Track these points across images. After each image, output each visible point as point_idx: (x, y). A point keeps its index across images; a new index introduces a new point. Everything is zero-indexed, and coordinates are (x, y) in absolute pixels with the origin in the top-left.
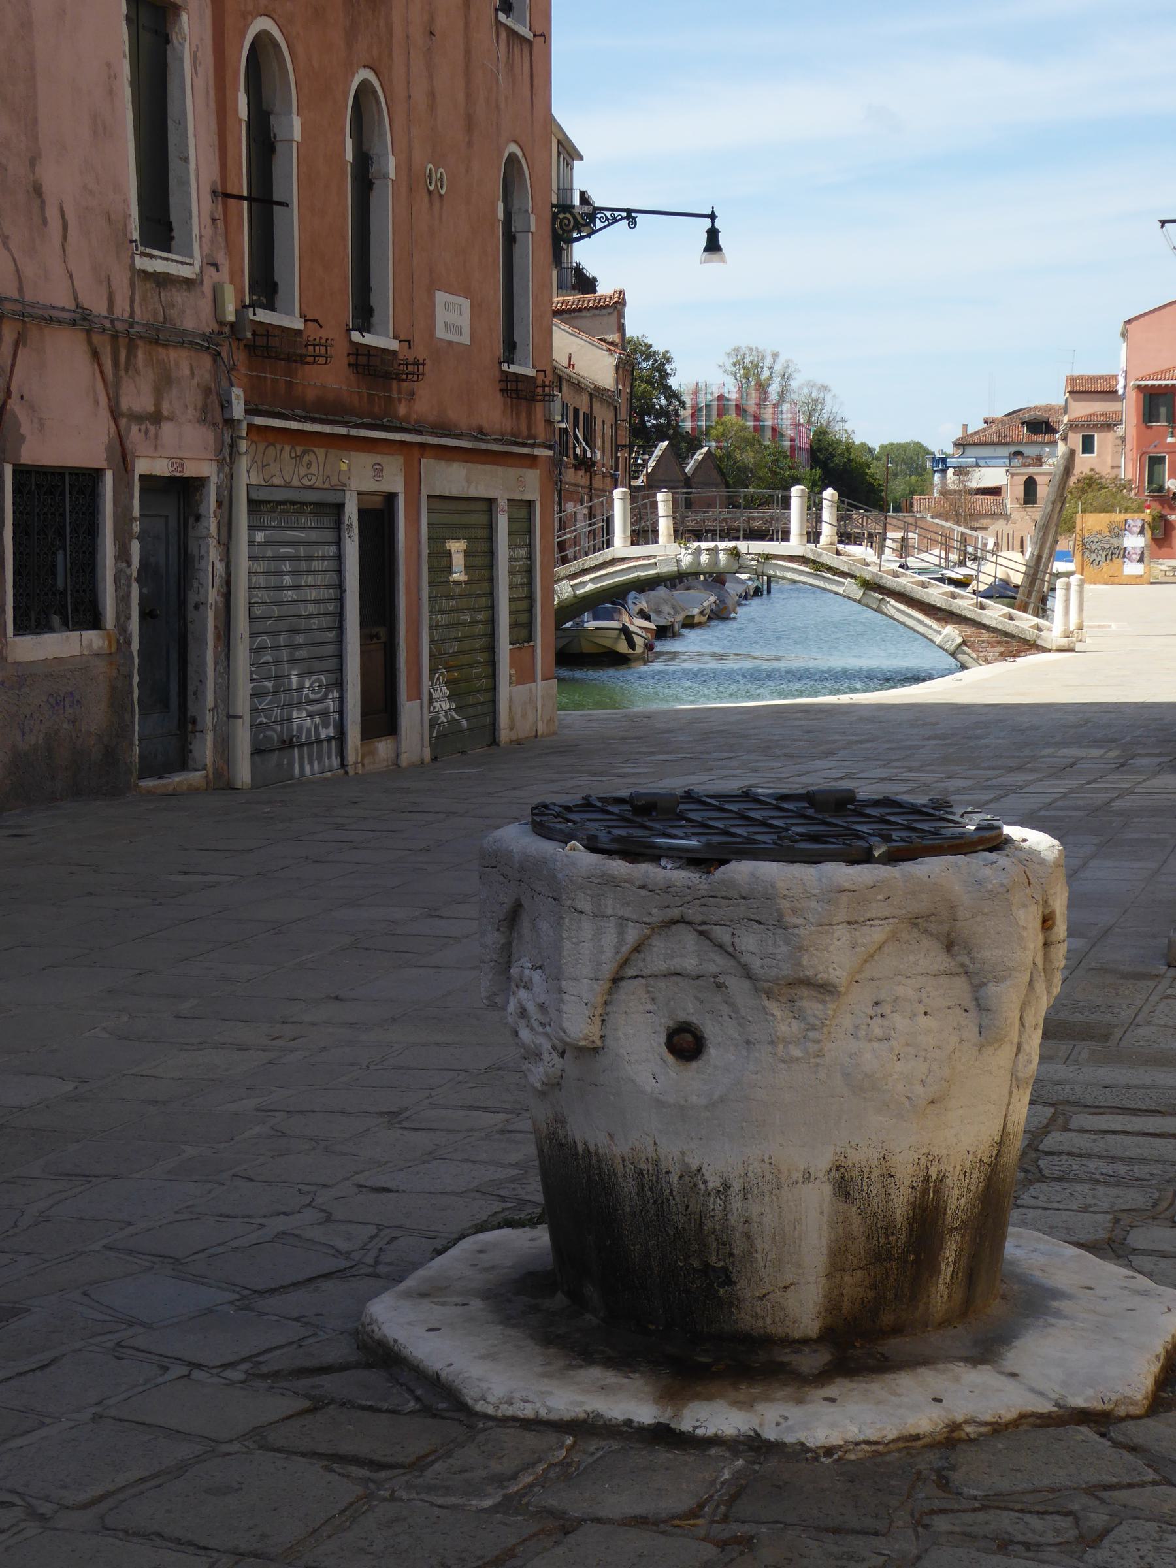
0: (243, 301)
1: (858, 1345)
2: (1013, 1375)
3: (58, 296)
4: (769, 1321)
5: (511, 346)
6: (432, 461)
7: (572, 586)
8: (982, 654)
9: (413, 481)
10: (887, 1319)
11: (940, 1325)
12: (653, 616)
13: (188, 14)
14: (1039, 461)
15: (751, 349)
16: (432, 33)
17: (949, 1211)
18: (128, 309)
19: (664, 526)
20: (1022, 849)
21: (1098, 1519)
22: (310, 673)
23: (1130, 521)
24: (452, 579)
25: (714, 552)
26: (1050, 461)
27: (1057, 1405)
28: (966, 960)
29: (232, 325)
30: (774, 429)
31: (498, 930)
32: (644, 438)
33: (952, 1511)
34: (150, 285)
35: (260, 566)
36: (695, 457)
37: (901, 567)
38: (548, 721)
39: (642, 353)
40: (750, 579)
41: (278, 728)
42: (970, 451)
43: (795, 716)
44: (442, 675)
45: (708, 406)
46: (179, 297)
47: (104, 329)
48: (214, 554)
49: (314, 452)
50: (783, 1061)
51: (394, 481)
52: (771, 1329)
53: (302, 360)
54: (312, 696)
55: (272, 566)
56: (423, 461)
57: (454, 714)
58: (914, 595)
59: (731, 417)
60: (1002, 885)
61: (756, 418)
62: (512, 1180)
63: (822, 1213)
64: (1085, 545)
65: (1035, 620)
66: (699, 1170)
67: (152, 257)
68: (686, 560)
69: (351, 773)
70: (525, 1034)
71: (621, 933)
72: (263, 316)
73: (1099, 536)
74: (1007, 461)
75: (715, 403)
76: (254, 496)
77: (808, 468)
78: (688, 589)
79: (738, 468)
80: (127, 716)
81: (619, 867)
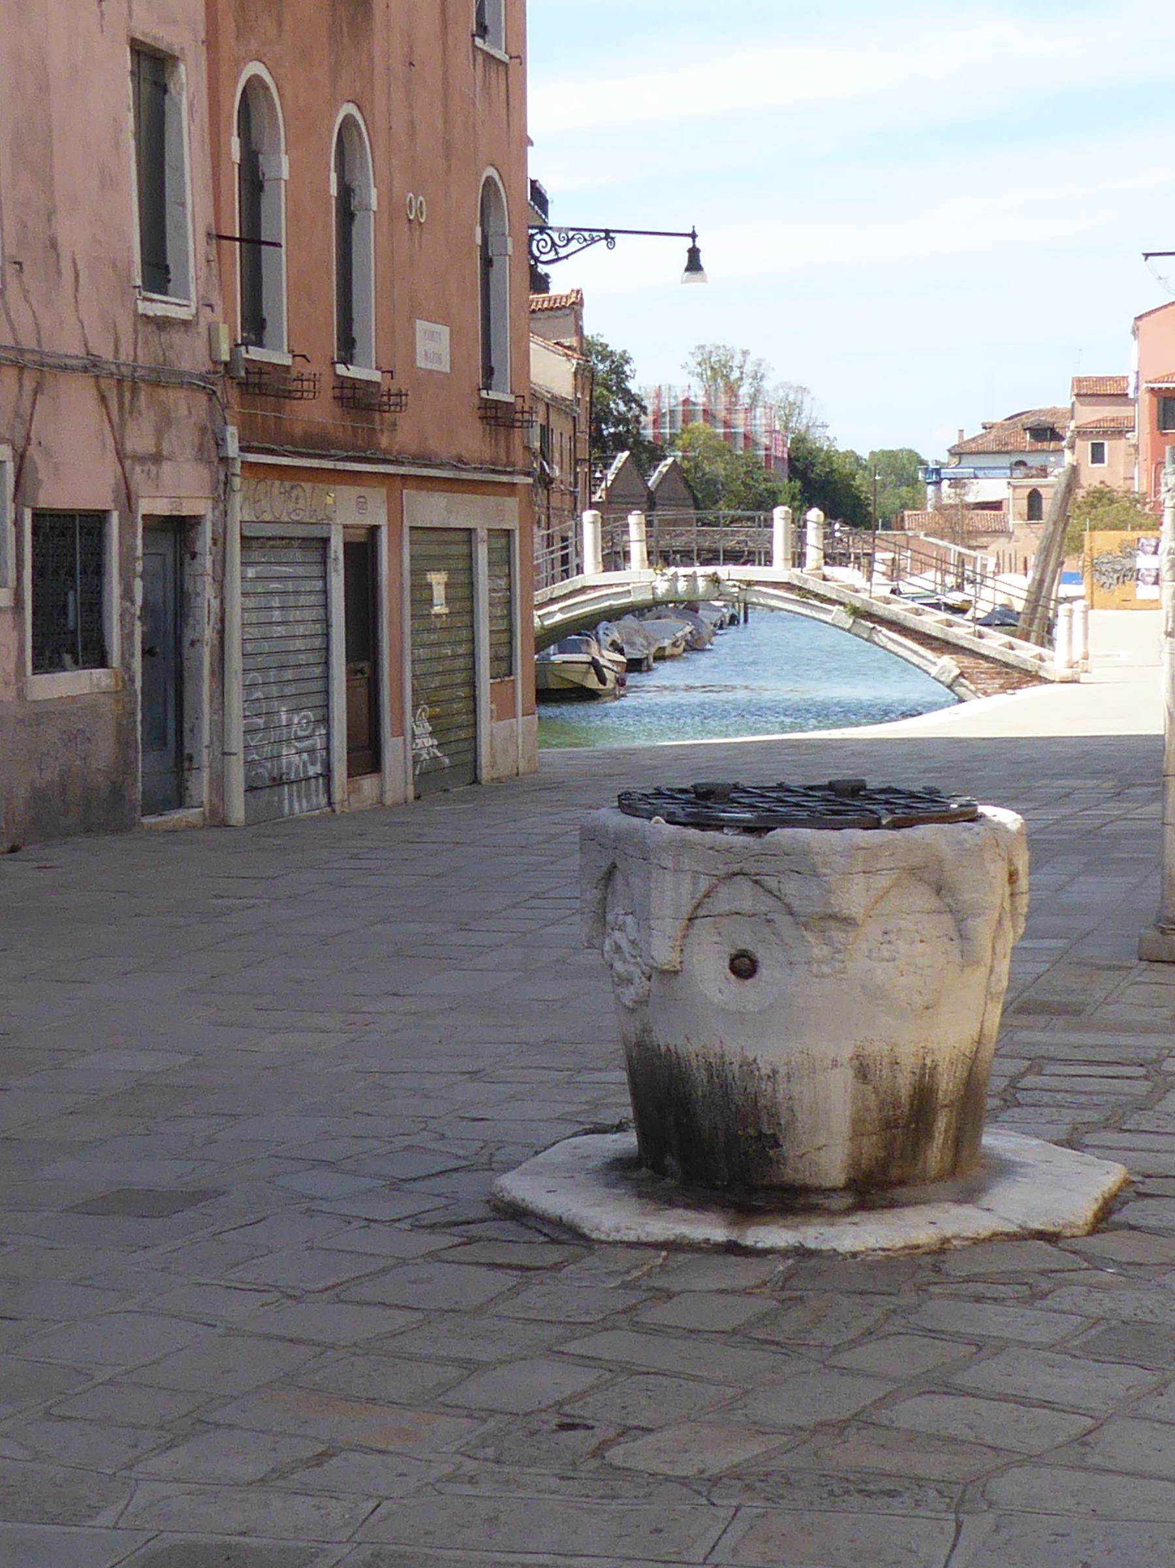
0: (235, 340)
1: (873, 1192)
2: (988, 1210)
3: (68, 345)
4: (807, 1173)
5: (488, 371)
6: (413, 492)
7: (539, 617)
8: (980, 686)
9: (396, 511)
10: (894, 1173)
11: (933, 1181)
12: (626, 649)
13: (185, 65)
14: (1043, 472)
15: (718, 347)
16: (411, 64)
17: (940, 1092)
18: (132, 353)
19: (637, 550)
20: (991, 821)
21: (1045, 1285)
22: (297, 710)
23: (1143, 540)
24: (433, 612)
25: (691, 578)
26: (1056, 472)
27: (1020, 1227)
28: (949, 900)
29: (226, 364)
30: (746, 437)
31: (596, 888)
32: (602, 447)
33: (943, 1283)
34: (151, 328)
35: (251, 603)
36: (659, 469)
37: (893, 592)
38: (530, 759)
39: (598, 353)
40: (725, 606)
41: (269, 765)
42: (967, 460)
43: (786, 751)
44: (425, 711)
45: (672, 412)
46: (177, 338)
47: (112, 374)
48: (209, 591)
49: (303, 488)
50: (817, 976)
51: (378, 515)
52: (809, 1181)
53: (289, 395)
54: (301, 733)
55: (263, 601)
56: (405, 491)
57: (436, 751)
58: (908, 624)
59: (699, 423)
60: (977, 845)
61: (727, 424)
62: (587, 1111)
63: (846, 1091)
64: (1094, 567)
65: (1038, 650)
66: (755, 1060)
67: (152, 300)
68: (662, 587)
69: (338, 812)
70: (619, 966)
71: (695, 883)
72: (255, 353)
73: (1110, 557)
74: (1008, 471)
75: (680, 408)
76: (247, 533)
77: (786, 481)
78: (659, 618)
79: (708, 481)
80: (131, 753)
81: (692, 833)
